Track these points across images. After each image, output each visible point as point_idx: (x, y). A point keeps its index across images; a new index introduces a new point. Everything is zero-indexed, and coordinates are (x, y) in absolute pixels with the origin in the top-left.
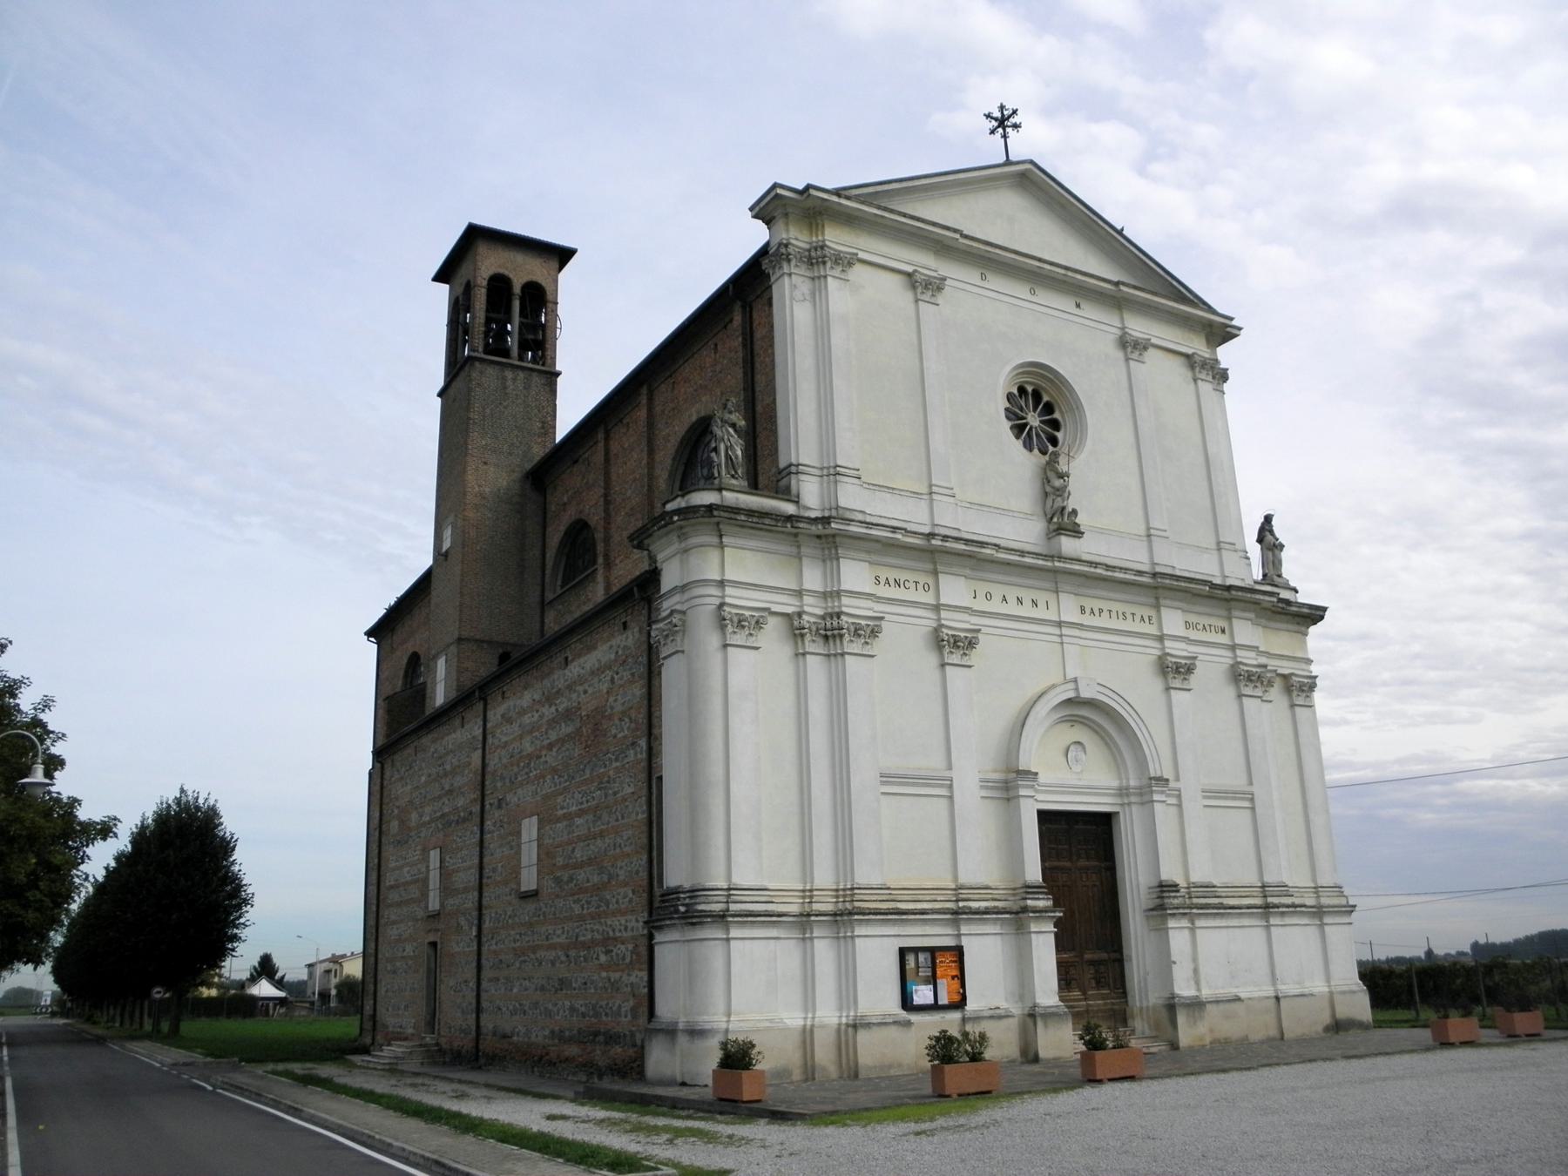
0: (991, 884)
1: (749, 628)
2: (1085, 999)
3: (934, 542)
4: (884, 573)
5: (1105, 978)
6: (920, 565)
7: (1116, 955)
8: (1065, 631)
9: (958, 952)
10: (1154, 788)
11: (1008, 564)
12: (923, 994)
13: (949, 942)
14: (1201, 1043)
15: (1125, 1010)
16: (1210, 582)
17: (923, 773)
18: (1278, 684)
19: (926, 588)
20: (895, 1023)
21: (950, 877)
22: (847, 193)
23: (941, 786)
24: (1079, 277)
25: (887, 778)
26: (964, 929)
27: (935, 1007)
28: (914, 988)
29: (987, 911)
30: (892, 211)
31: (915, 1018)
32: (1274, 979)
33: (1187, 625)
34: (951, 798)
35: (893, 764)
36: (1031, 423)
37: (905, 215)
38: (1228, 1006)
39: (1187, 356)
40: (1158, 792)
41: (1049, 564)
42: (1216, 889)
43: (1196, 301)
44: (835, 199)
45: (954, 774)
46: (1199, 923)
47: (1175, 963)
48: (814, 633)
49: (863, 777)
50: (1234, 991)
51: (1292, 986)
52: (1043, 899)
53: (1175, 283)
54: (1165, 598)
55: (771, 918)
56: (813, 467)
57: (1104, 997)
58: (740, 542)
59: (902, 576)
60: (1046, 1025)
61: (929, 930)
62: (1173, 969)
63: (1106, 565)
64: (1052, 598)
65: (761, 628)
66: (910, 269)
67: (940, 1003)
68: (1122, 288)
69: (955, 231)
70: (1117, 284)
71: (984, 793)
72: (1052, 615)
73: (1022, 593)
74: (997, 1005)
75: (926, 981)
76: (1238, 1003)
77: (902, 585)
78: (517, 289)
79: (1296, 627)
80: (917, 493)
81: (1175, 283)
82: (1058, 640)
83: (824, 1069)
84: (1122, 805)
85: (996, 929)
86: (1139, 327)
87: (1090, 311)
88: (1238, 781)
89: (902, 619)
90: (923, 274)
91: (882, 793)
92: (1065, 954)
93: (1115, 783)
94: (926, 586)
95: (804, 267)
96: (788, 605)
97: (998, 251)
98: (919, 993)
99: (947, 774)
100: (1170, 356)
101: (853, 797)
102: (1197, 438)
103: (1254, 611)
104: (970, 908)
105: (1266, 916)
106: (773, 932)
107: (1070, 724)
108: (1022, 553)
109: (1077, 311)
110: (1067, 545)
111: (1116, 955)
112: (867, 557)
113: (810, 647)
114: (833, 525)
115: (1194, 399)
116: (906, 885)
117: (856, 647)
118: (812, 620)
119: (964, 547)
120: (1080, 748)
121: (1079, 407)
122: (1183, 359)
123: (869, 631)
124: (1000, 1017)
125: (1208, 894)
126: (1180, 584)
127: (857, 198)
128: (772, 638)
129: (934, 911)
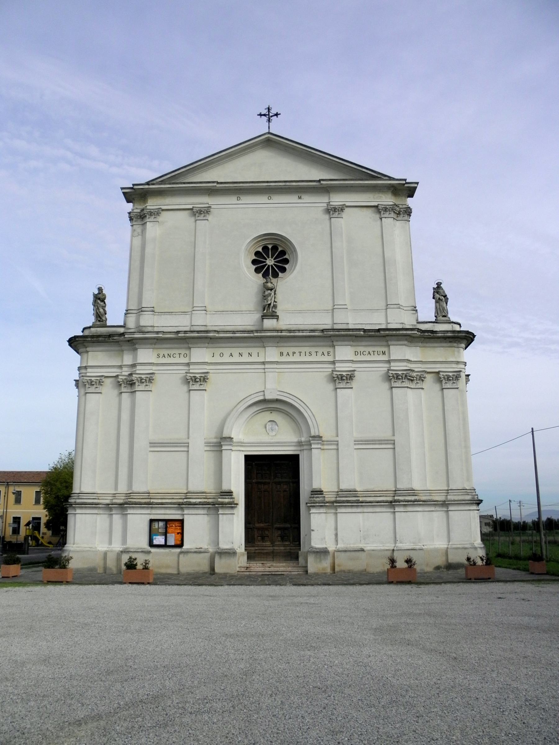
0: (208, 491)
1: (417, 380)
2: (273, 546)
3: (180, 335)
4: (162, 352)
5: (287, 536)
6: (182, 346)
7: (297, 525)
8: (267, 366)
9: (182, 522)
10: (311, 442)
11: (273, 337)
12: (159, 540)
13: (179, 517)
14: (323, 572)
15: (298, 553)
16: (363, 329)
17: (172, 441)
18: (429, 378)
19: (384, 353)
20: (142, 552)
21: (185, 488)
22: (153, 182)
23: (391, 444)
24: (294, 184)
25: (153, 444)
26: (186, 512)
27: (165, 546)
28: (154, 537)
29: (200, 504)
30: (177, 183)
31: (153, 550)
32: (395, 541)
33: (356, 353)
34: (338, 449)
35: (154, 437)
36: (270, 264)
37: (184, 183)
38: (353, 553)
39: (376, 207)
40: (314, 443)
41: (252, 335)
42: (357, 493)
43: (379, 176)
44: (147, 187)
45: (190, 441)
46: (339, 510)
47: (313, 530)
48: (148, 382)
49: (141, 443)
50: (361, 546)
51: (407, 544)
52: (229, 498)
53: (364, 170)
54: (337, 341)
55: (94, 506)
56: (135, 310)
57: (284, 546)
58: (94, 349)
59: (171, 352)
60: (220, 557)
61: (168, 511)
62: (312, 534)
63: (163, 332)
64: (331, 350)
65: (206, 381)
66: (191, 207)
67: (168, 544)
68: (322, 182)
69: (213, 182)
70: (319, 181)
71: (208, 449)
72: (261, 360)
73: (250, 350)
74: (201, 547)
75: (161, 534)
76: (363, 552)
77: (381, 352)
78: (284, 257)
79: (449, 344)
80: (185, 312)
81: (364, 170)
82: (263, 371)
83: (110, 569)
84: (301, 450)
85: (205, 511)
86: (337, 199)
87: (307, 198)
88: (387, 435)
89: (221, 371)
90: (382, 205)
91: (355, 449)
92: (263, 524)
93: (296, 440)
94: (185, 355)
95: (139, 220)
96: (114, 372)
97: (241, 185)
98: (156, 539)
99: (336, 439)
100: (365, 209)
101: (135, 453)
102: (379, 250)
103: (406, 340)
104: (191, 502)
105: (393, 507)
106: (96, 511)
107: (269, 412)
108: (252, 332)
109: (300, 201)
110: (269, 323)
111: (297, 525)
112: (151, 346)
113: (123, 390)
114: (126, 336)
115: (379, 228)
116: (160, 491)
117: (142, 387)
118: (124, 378)
119: (197, 335)
120: (274, 423)
121: (295, 250)
122: (373, 209)
123: (150, 379)
124: (200, 552)
125: (348, 495)
126: (340, 333)
127: (162, 182)
128: (108, 388)
129: (171, 503)
